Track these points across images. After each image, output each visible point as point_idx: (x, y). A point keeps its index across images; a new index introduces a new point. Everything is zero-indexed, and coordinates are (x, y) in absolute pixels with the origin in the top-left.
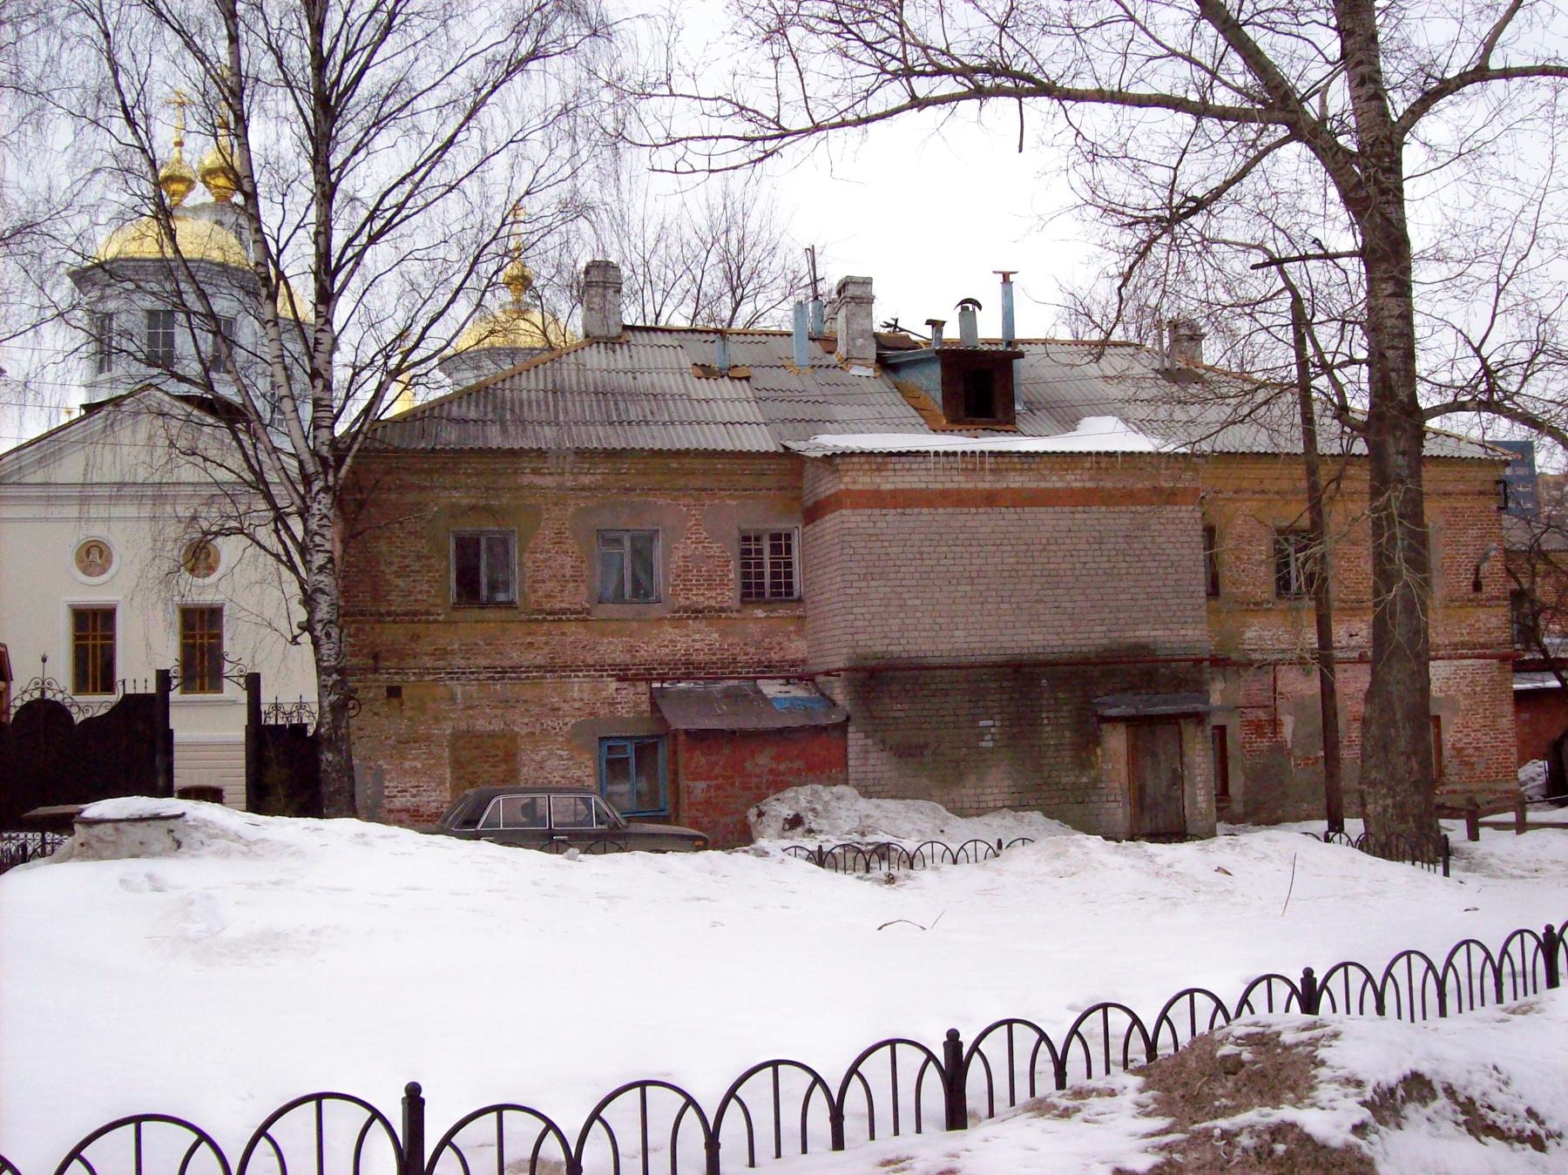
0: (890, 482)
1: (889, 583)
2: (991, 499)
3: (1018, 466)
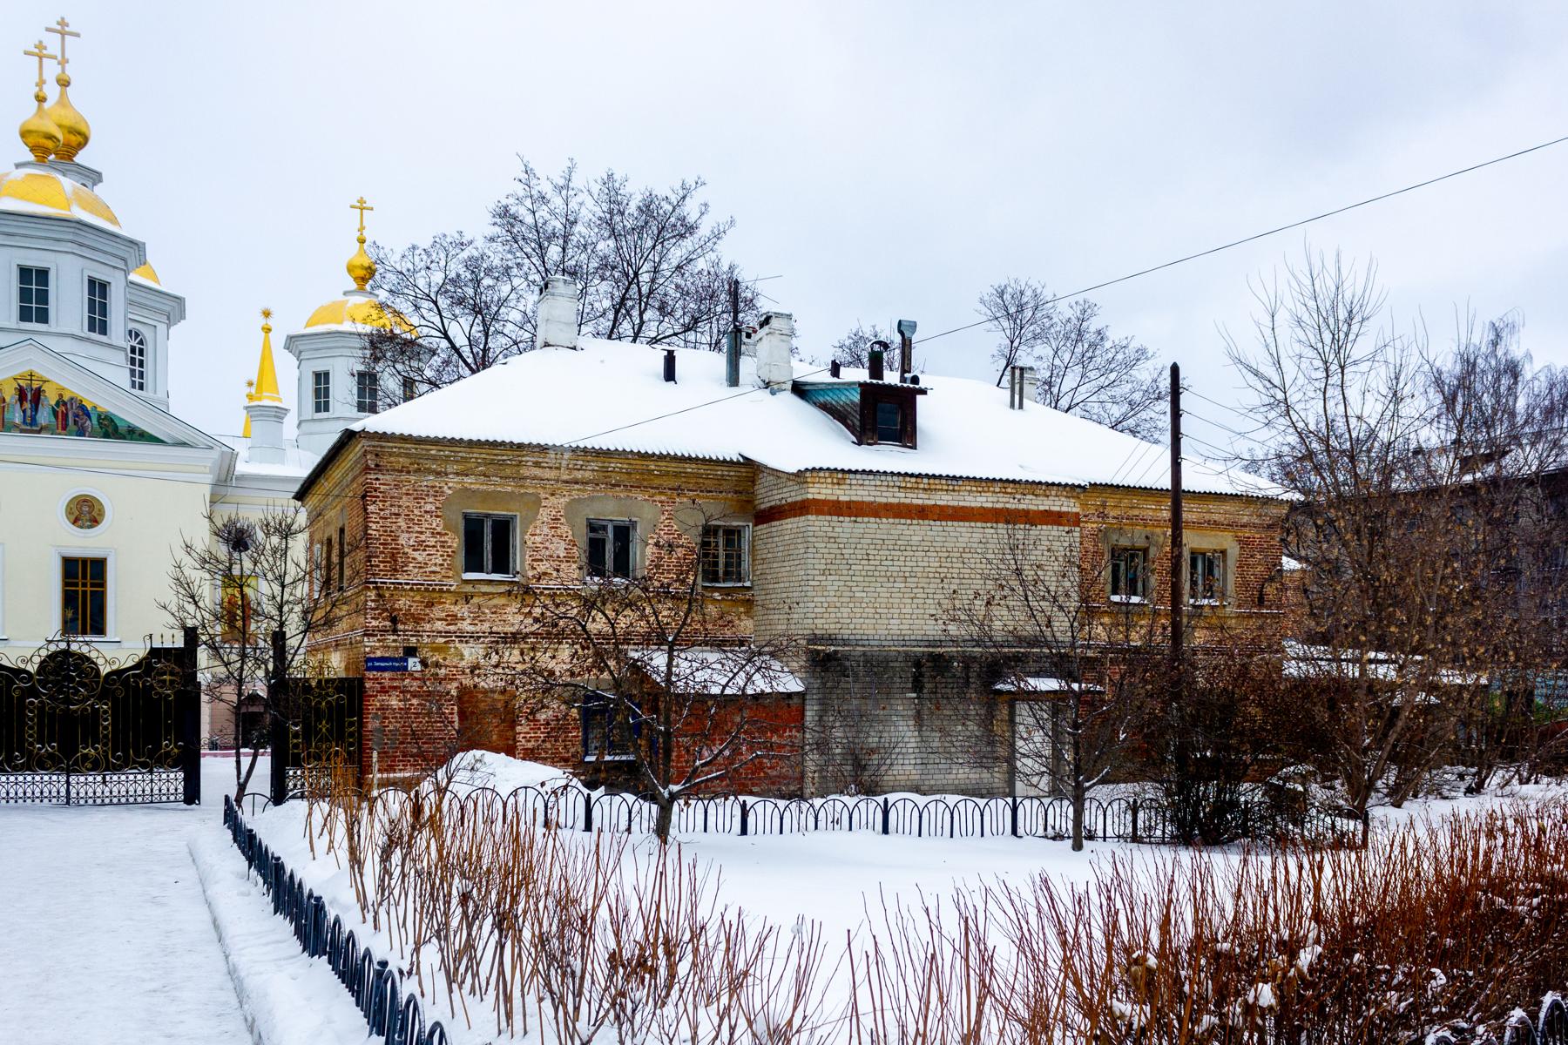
0: (843, 494)
1: (841, 578)
2: (922, 513)
3: (945, 487)
